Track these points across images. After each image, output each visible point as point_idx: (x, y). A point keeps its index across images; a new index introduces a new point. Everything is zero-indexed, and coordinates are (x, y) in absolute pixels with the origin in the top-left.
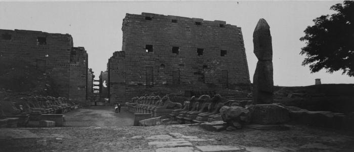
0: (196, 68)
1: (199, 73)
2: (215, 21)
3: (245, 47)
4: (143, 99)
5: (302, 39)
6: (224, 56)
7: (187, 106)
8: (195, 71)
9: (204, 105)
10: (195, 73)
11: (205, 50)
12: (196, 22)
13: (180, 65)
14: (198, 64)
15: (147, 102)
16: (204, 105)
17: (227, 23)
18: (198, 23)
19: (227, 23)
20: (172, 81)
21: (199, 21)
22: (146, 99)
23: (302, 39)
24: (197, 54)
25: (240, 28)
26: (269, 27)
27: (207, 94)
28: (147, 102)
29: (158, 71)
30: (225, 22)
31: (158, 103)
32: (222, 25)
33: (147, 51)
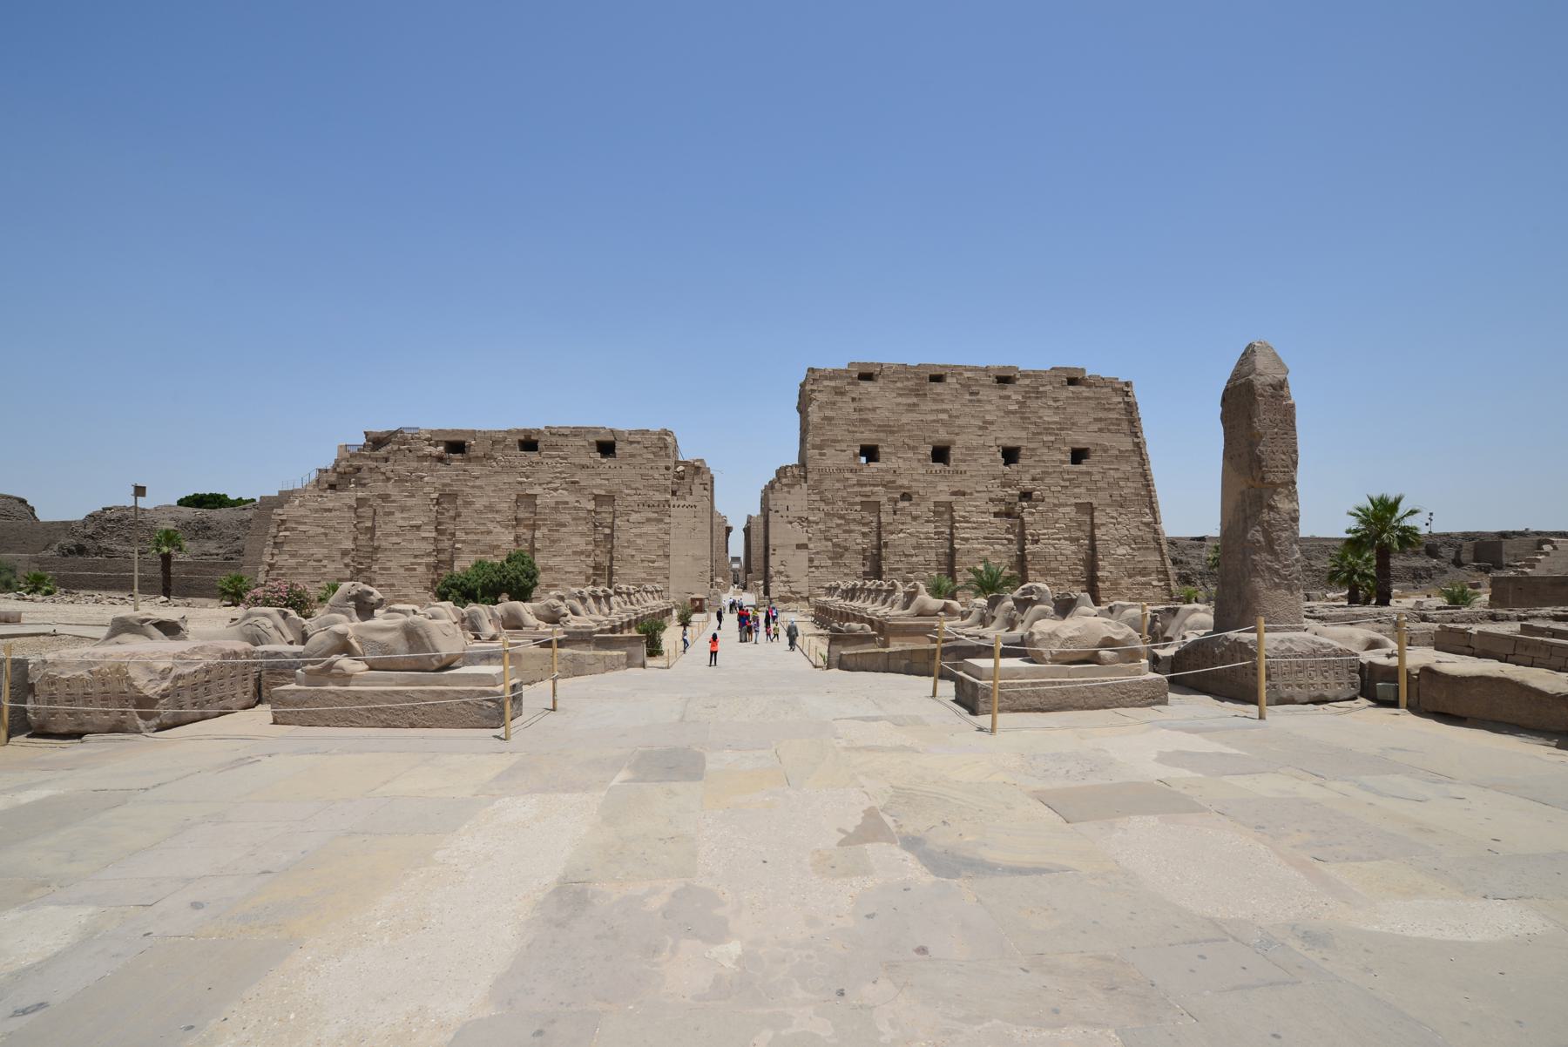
1: (1008, 515)
13: (954, 494)
17: (1087, 374)
19: (1087, 374)
30: (1083, 370)
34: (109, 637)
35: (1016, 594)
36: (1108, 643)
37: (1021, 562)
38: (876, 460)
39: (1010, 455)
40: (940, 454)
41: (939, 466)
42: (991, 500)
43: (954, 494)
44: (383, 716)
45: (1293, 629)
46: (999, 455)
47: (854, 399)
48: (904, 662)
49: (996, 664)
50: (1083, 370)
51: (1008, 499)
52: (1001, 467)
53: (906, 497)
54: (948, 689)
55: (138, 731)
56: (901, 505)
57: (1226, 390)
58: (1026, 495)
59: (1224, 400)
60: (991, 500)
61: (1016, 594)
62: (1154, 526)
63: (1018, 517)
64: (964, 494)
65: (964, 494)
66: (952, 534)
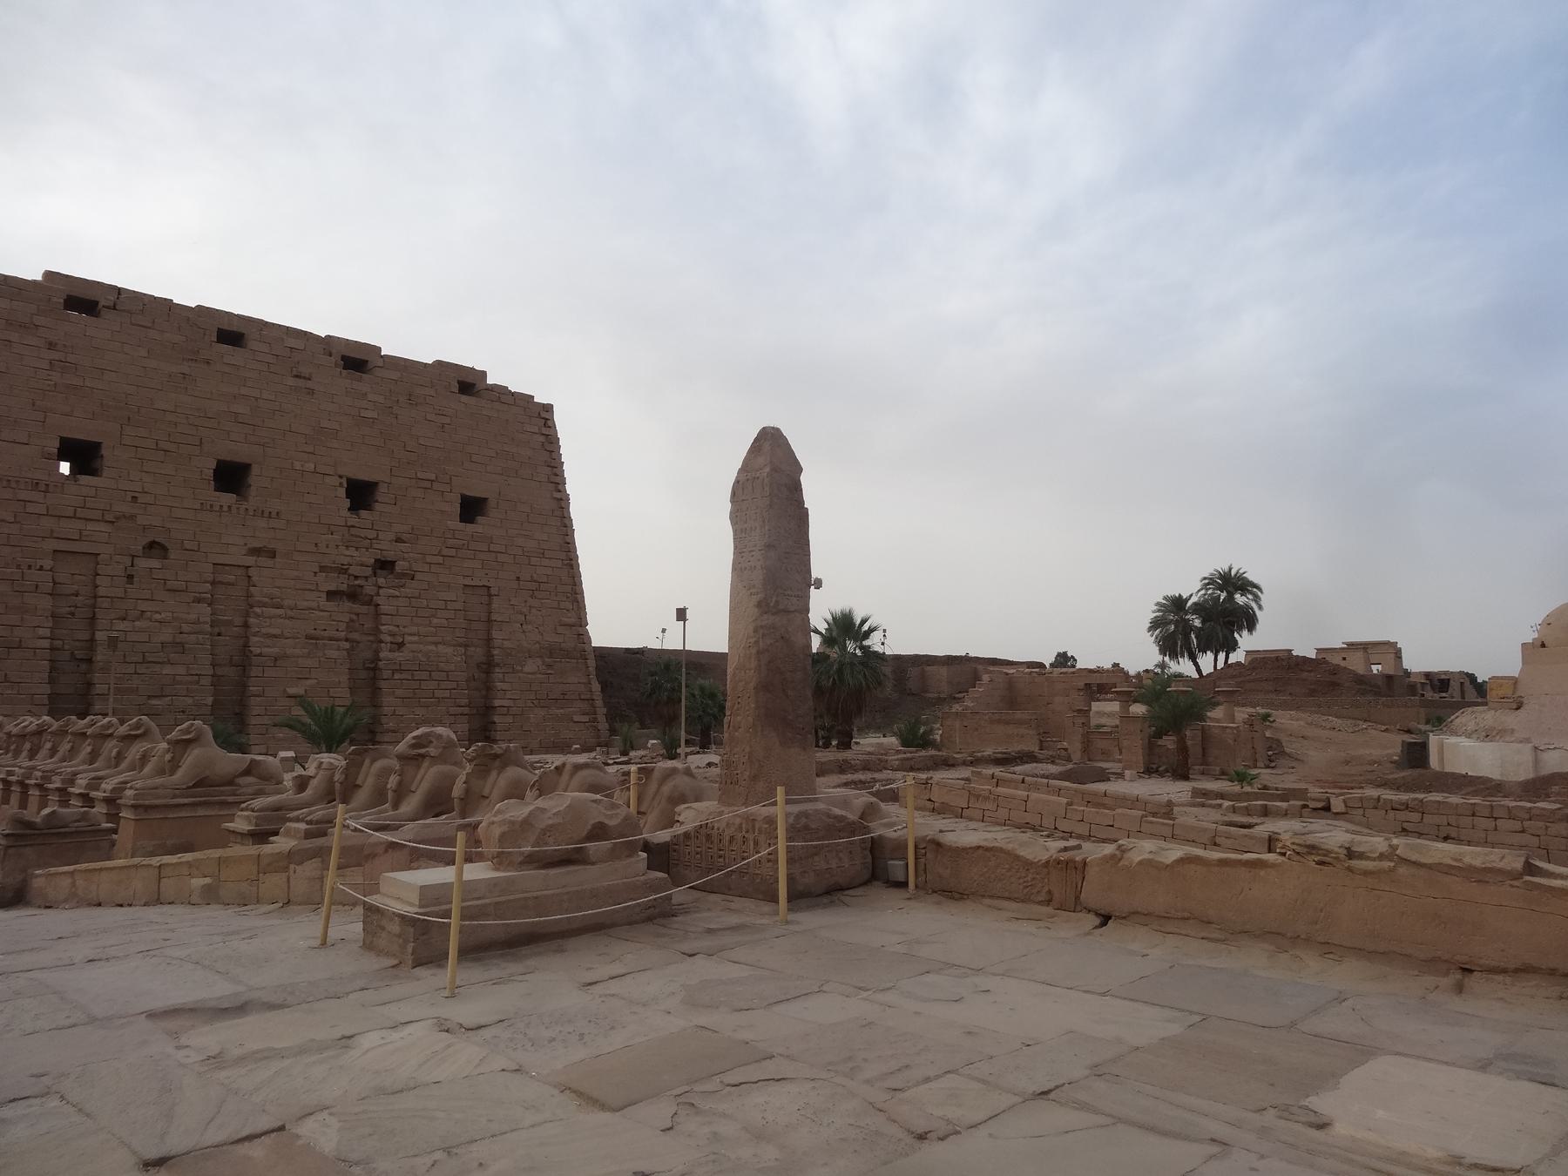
0: (343, 570)
1: (353, 595)
2: (439, 363)
3: (569, 488)
4: (40, 732)
5: (770, 494)
6: (472, 521)
7: (331, 781)
8: (332, 588)
9: (426, 778)
10: (331, 595)
11: (382, 489)
12: (344, 358)
13: (256, 552)
14: (352, 552)
15: (65, 747)
16: (426, 778)
17: (490, 381)
18: (357, 360)
19: (490, 381)
20: (207, 628)
21: (470, 380)
22: (62, 732)
23: (770, 494)
24: (347, 503)
25: (548, 408)
26: (798, 469)
27: (441, 723)
28: (65, 747)
29: (130, 577)
30: (484, 374)
31: (144, 759)
32: (468, 383)
33: (65, 468)
34: (521, 863)
35: (401, 747)
36: (599, 832)
37: (369, 677)
38: (94, 472)
39: (360, 494)
40: (231, 477)
41: (228, 498)
42: (323, 569)
43: (256, 552)
44: (1229, 842)
45: (810, 800)
46: (342, 492)
47: (51, 346)
48: (198, 882)
49: (460, 873)
50: (484, 374)
51: (354, 570)
52: (345, 513)
53: (155, 548)
54: (350, 927)
55: (684, 910)
56: (143, 563)
57: (737, 482)
58: (385, 565)
59: (734, 494)
60: (323, 569)
61: (401, 747)
62: (583, 637)
63: (370, 602)
64: (272, 554)
65: (272, 554)
66: (246, 625)
